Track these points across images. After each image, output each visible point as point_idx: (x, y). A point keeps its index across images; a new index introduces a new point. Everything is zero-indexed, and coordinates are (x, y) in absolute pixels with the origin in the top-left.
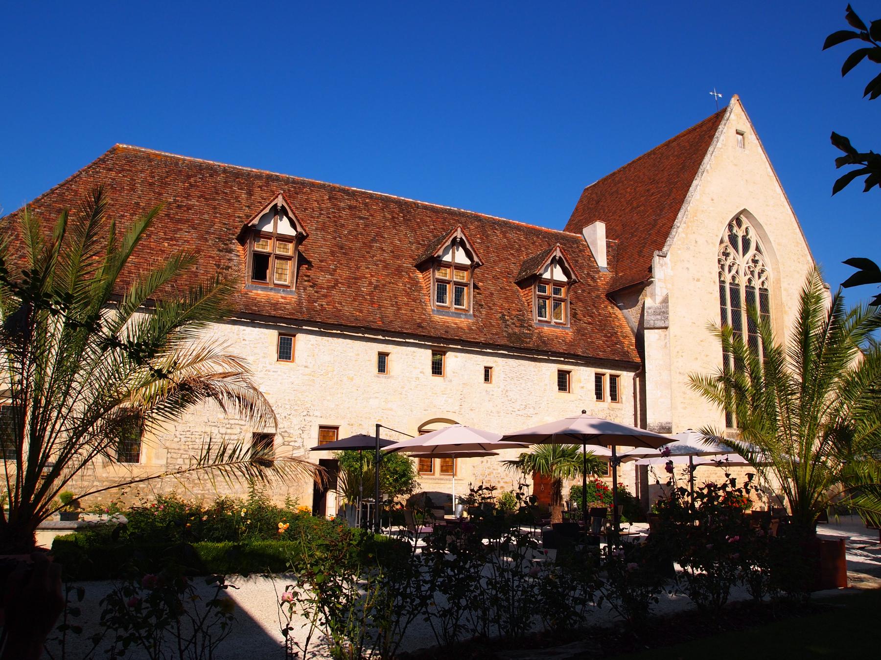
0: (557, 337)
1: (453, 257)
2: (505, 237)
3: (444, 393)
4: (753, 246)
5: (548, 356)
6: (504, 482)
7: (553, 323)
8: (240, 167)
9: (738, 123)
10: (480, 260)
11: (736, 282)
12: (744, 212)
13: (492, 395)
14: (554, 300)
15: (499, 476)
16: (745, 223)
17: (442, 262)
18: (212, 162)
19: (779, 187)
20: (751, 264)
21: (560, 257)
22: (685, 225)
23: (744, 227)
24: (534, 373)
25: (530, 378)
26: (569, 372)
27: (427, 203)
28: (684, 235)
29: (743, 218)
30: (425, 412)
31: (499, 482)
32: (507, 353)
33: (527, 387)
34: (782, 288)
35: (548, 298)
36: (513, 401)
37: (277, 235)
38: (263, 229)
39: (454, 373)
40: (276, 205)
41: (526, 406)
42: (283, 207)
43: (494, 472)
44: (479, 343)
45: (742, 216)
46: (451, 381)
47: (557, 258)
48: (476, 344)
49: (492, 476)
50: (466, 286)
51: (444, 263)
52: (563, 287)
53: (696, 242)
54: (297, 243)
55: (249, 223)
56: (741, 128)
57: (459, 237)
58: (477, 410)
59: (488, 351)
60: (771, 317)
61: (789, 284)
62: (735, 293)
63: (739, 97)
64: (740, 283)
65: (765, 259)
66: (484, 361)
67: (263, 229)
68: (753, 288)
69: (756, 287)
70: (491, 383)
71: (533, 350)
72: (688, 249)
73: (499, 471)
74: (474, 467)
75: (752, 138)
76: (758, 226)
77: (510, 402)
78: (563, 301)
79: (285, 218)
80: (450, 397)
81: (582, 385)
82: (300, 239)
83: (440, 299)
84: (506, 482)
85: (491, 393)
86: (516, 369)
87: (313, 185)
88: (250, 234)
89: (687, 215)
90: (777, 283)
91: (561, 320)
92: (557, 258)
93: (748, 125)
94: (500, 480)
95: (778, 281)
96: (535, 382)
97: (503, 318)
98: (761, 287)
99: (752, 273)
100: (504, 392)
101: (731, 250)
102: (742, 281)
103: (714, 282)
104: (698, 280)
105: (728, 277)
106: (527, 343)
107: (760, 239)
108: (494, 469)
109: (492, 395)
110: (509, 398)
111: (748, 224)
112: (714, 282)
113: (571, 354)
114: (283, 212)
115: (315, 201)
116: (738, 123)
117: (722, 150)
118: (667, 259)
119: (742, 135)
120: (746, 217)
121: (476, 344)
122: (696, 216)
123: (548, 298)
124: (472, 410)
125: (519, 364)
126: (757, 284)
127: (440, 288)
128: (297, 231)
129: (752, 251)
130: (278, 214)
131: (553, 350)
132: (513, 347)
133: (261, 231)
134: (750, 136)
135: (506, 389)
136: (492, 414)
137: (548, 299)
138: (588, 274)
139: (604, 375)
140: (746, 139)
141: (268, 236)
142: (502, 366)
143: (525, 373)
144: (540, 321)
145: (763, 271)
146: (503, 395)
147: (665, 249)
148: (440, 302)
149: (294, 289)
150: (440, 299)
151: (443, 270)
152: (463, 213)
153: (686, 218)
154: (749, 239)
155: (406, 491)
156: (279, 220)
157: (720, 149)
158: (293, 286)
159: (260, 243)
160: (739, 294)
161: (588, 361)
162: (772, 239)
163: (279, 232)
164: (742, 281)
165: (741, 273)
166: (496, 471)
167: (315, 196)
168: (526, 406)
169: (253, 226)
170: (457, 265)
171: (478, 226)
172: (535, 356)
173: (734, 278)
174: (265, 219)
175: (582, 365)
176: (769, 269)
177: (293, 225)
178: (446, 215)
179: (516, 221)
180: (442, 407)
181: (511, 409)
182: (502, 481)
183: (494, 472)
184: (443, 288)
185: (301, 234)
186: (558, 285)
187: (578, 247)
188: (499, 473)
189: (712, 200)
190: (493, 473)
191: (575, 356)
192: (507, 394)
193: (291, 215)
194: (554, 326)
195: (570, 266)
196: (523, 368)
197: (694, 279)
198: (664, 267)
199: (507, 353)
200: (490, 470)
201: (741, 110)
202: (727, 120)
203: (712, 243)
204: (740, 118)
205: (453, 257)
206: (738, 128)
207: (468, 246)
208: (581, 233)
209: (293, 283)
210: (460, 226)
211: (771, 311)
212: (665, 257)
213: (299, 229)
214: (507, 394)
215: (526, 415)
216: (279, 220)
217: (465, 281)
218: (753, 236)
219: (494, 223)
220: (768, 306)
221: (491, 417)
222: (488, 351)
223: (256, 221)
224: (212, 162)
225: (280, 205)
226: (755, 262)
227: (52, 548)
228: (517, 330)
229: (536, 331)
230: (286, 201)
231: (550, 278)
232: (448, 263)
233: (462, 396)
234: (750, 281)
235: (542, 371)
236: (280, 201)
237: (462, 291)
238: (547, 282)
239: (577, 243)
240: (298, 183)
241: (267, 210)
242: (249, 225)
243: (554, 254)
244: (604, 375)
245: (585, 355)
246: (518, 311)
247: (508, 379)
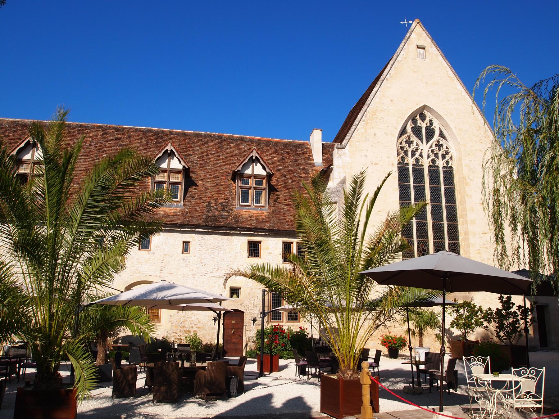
1: (33, 155)
2: (238, 148)
3: (147, 262)
4: (437, 133)
5: (239, 231)
6: (196, 327)
7: (252, 207)
8: (46, 121)
9: (419, 40)
10: (271, 171)
11: (450, 165)
12: (424, 107)
13: (189, 262)
14: (254, 189)
15: (192, 322)
16: (429, 116)
18: (27, 120)
19: (460, 85)
20: (434, 148)
22: (364, 122)
23: (428, 119)
24: (227, 244)
25: (222, 248)
26: (260, 242)
27: (180, 131)
28: (363, 131)
29: (426, 112)
30: (132, 277)
31: (192, 327)
32: (203, 230)
33: (220, 255)
34: (463, 165)
35: (250, 188)
36: (207, 266)
37: (169, 170)
38: (24, 158)
39: (156, 247)
41: (218, 269)
43: (188, 319)
44: (177, 224)
45: (425, 111)
46: (154, 253)
48: (175, 225)
49: (186, 322)
50: (180, 184)
53: (375, 135)
55: (235, 170)
56: (421, 44)
58: (175, 274)
59: (187, 229)
60: (456, 189)
61: (471, 161)
62: (418, 172)
63: (420, 20)
64: (423, 164)
65: (451, 144)
66: (182, 237)
68: (438, 167)
69: (439, 166)
70: (189, 253)
71: (224, 227)
72: (367, 140)
73: (193, 319)
74: (171, 316)
75: (433, 50)
76: (439, 117)
77: (205, 267)
78: (264, 190)
79: (258, 164)
80: (152, 265)
81: (269, 251)
82: (269, 176)
83: (258, 201)
84: (199, 327)
85: (188, 261)
86: (210, 242)
87: (94, 127)
88: (237, 176)
89: (366, 115)
90: (459, 161)
91: (177, 198)
93: (429, 40)
94: (193, 326)
95: (460, 159)
96: (226, 251)
97: (209, 206)
98: (445, 165)
99: (436, 155)
100: (199, 259)
101: (414, 138)
102: (426, 163)
103: (393, 164)
104: (376, 164)
105: (410, 161)
106: (220, 222)
107: (442, 126)
108: (188, 318)
109: (189, 262)
110: (203, 264)
111: (432, 117)
112: (393, 164)
113: (258, 228)
114: (256, 161)
115: (90, 137)
116: (419, 40)
117: (402, 62)
118: (346, 150)
119: (424, 49)
120: (428, 112)
121: (175, 225)
122: (375, 115)
123: (250, 188)
124: (170, 274)
125: (213, 238)
126: (441, 163)
127: (258, 193)
128: (267, 172)
129: (436, 137)
130: (254, 162)
131: (242, 226)
132: (206, 226)
133: (244, 174)
134: (430, 49)
135: (201, 257)
136: (187, 276)
137: (250, 189)
138: (303, 169)
139: (292, 243)
140: (427, 51)
141: (164, 171)
142: (196, 240)
143: (217, 244)
144: (256, 206)
145: (447, 153)
146: (198, 262)
147: (344, 142)
150: (258, 201)
151: (162, 174)
152: (209, 134)
153: (365, 117)
154: (433, 129)
155: (114, 334)
156: (255, 166)
157: (401, 61)
159: (23, 167)
160: (423, 172)
161: (276, 233)
162: (452, 126)
164: (426, 163)
165: (425, 155)
166: (190, 319)
167: (93, 134)
168: (218, 269)
169: (238, 171)
170: (172, 170)
171: (217, 143)
172: (227, 232)
173: (417, 160)
174: (245, 166)
175: (270, 236)
176: (453, 151)
177: (264, 168)
178: (192, 137)
179: (71, 122)
180: (146, 273)
181: (205, 272)
182: (195, 327)
183: (188, 319)
184: (246, 192)
186: (258, 178)
187: (302, 150)
188: (192, 321)
189: (392, 101)
190: (187, 320)
191: (263, 230)
192: (202, 261)
193: (262, 162)
194: (254, 209)
196: (216, 241)
197: (372, 163)
198: (342, 157)
199: (203, 230)
200: (185, 318)
201: (422, 30)
202: (408, 39)
203: (391, 134)
204: (421, 36)
205: (169, 164)
206: (418, 44)
208: (309, 140)
211: (455, 183)
212: (344, 148)
213: (268, 170)
214: (202, 261)
215: (218, 276)
217: (179, 181)
218: (437, 126)
219: (232, 139)
220: (453, 180)
221: (187, 278)
222: (187, 229)
223: (240, 168)
224: (27, 120)
225: (254, 156)
226: (439, 146)
227: (425, 359)
229: (234, 213)
230: (258, 154)
232: (164, 169)
233: (163, 264)
234: (433, 161)
235: (233, 242)
236: (254, 154)
238: (249, 176)
239: (302, 148)
240: (83, 127)
241: (246, 161)
243: (251, 155)
244: (292, 243)
245: (271, 228)
246: (225, 199)
247: (203, 250)
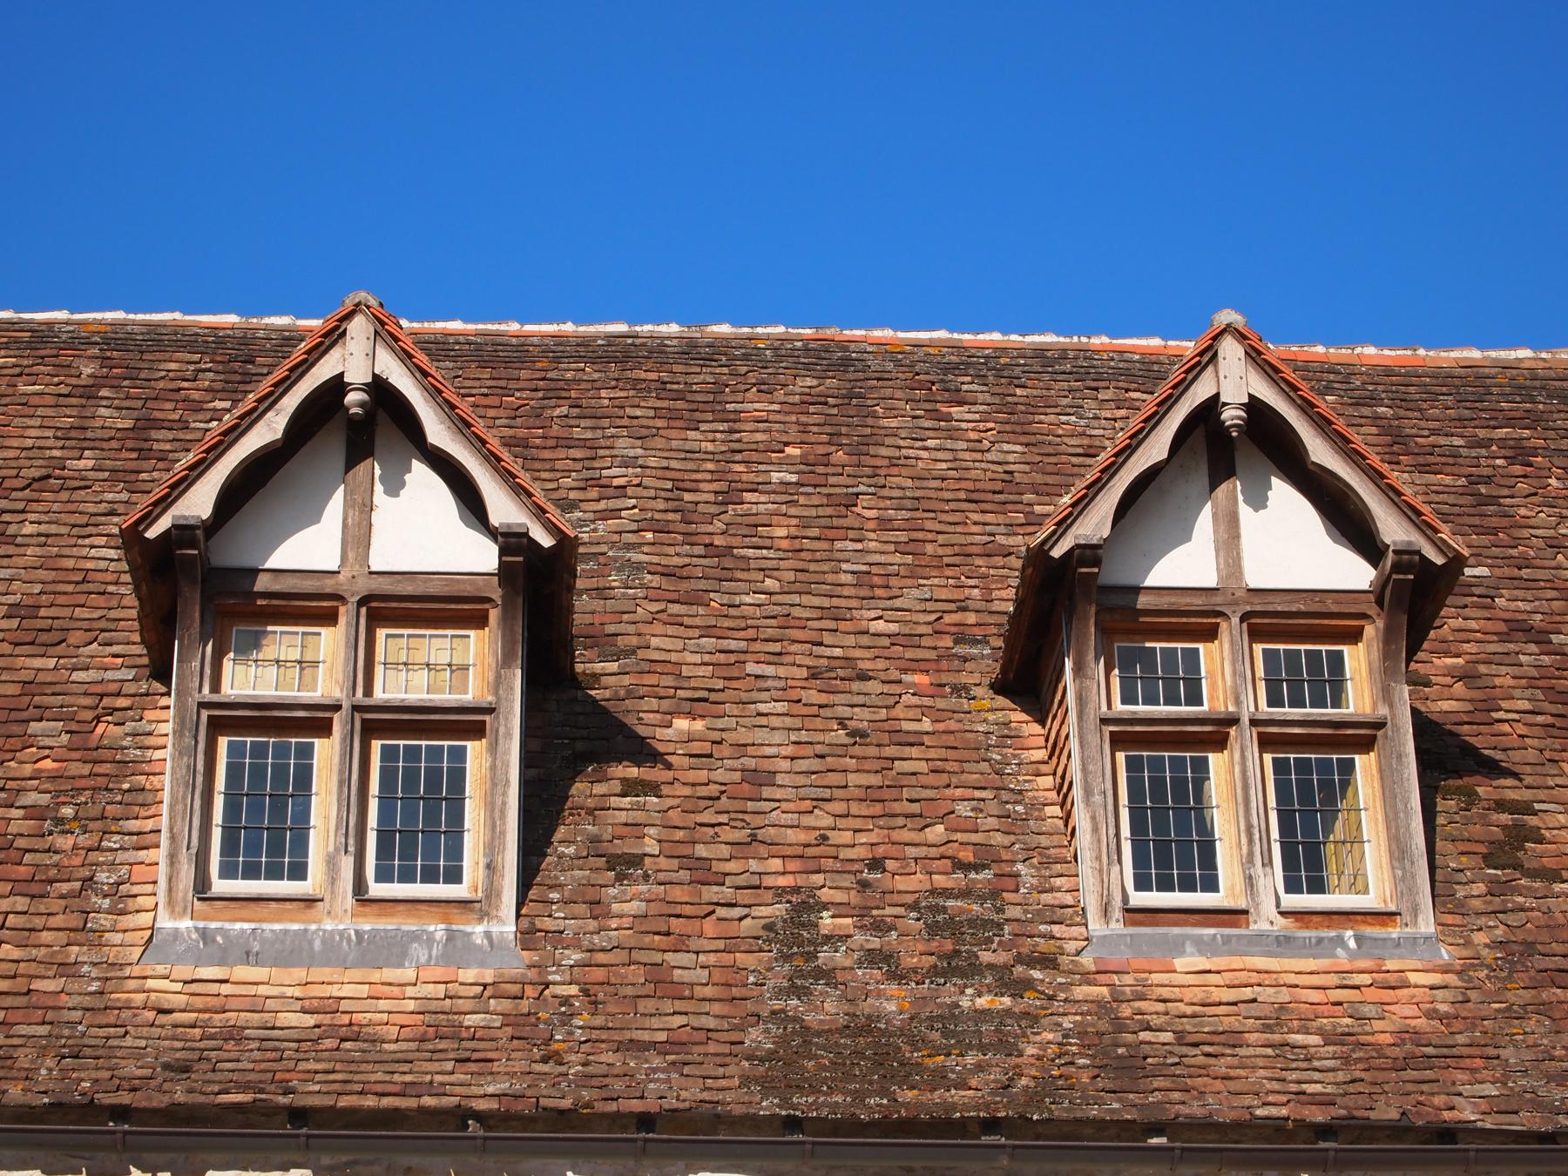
0: (1277, 1018)
10: (539, 512)
17: (262, 583)
21: (1254, 406)
37: (364, 586)
40: (1212, 405)
42: (1254, 406)
47: (1232, 416)
51: (1164, 602)
52: (1354, 636)
54: (1388, 637)
57: (358, 374)
67: (1152, 580)
92: (1232, 416)
106: (940, 1078)
131: (1195, 1109)
144: (1301, 916)
148: (1165, 885)
149: (1426, 924)
151: (283, 641)
158: (1415, 911)
163: (1256, 577)
170: (385, 586)
185: (1409, 560)
194: (1283, 943)
195: (1354, 457)
205: (358, 536)
207: (1320, 452)
209: (1412, 891)
210: (1228, 329)
213: (503, 508)
216: (379, 488)
223: (1095, 525)
228: (892, 1003)
229: (1080, 992)
231: (1211, 581)
232: (1198, 602)
237: (1338, 784)
241: (1156, 449)
242: (1057, 553)
